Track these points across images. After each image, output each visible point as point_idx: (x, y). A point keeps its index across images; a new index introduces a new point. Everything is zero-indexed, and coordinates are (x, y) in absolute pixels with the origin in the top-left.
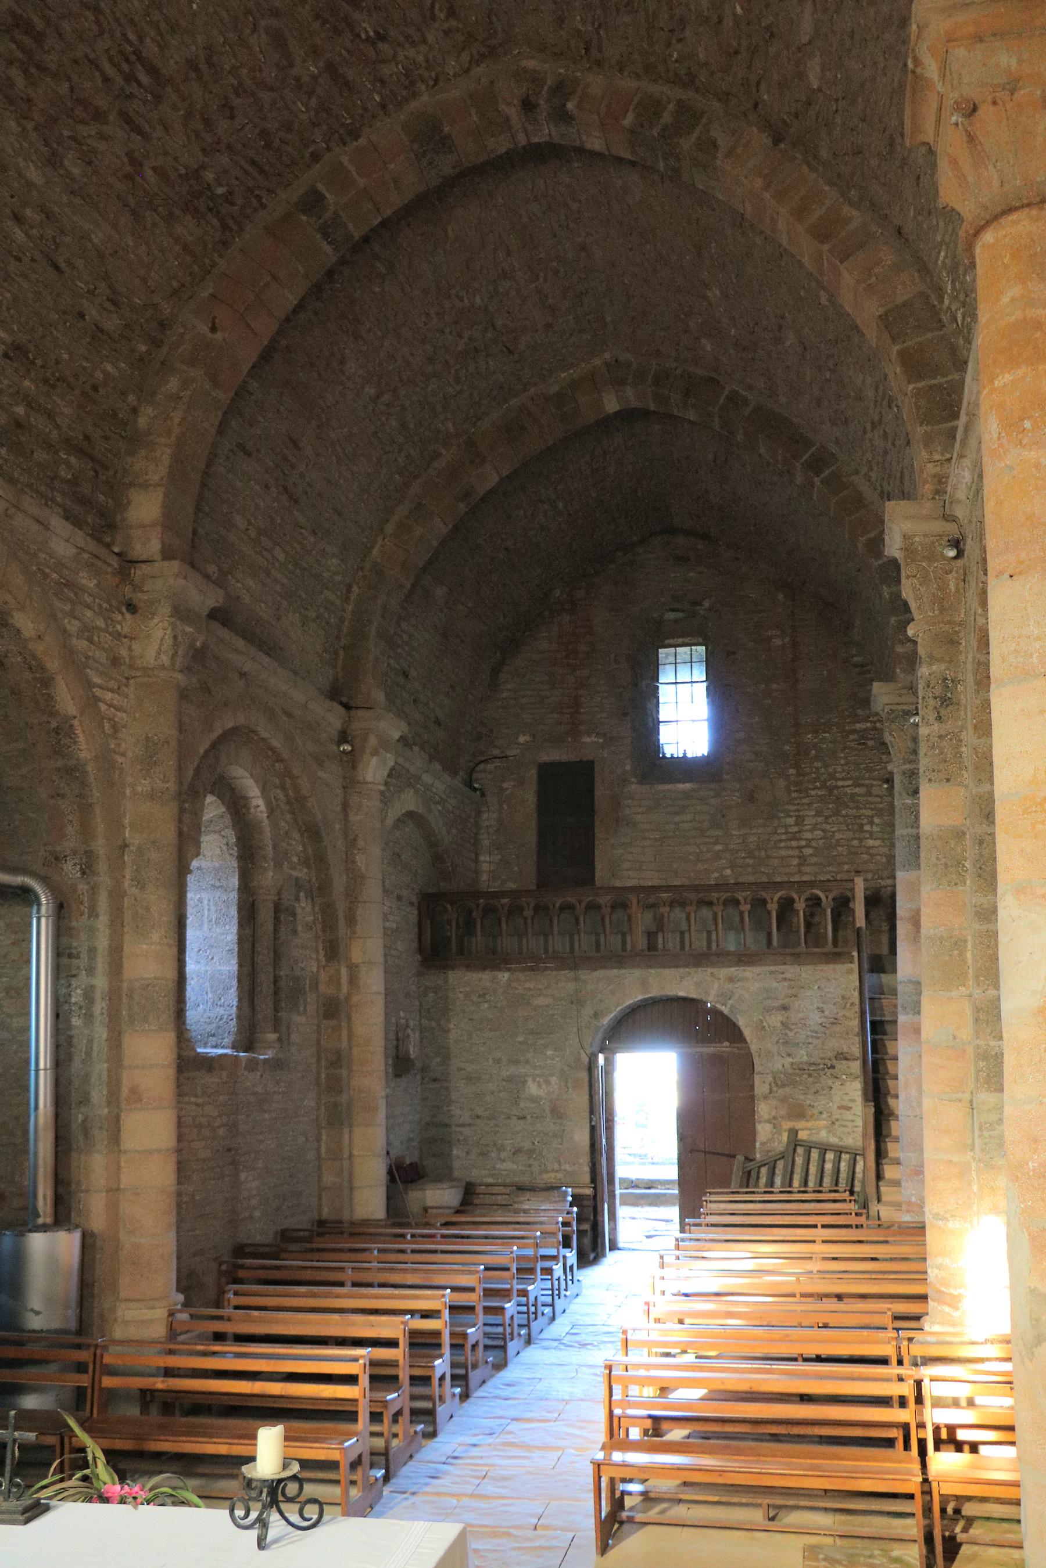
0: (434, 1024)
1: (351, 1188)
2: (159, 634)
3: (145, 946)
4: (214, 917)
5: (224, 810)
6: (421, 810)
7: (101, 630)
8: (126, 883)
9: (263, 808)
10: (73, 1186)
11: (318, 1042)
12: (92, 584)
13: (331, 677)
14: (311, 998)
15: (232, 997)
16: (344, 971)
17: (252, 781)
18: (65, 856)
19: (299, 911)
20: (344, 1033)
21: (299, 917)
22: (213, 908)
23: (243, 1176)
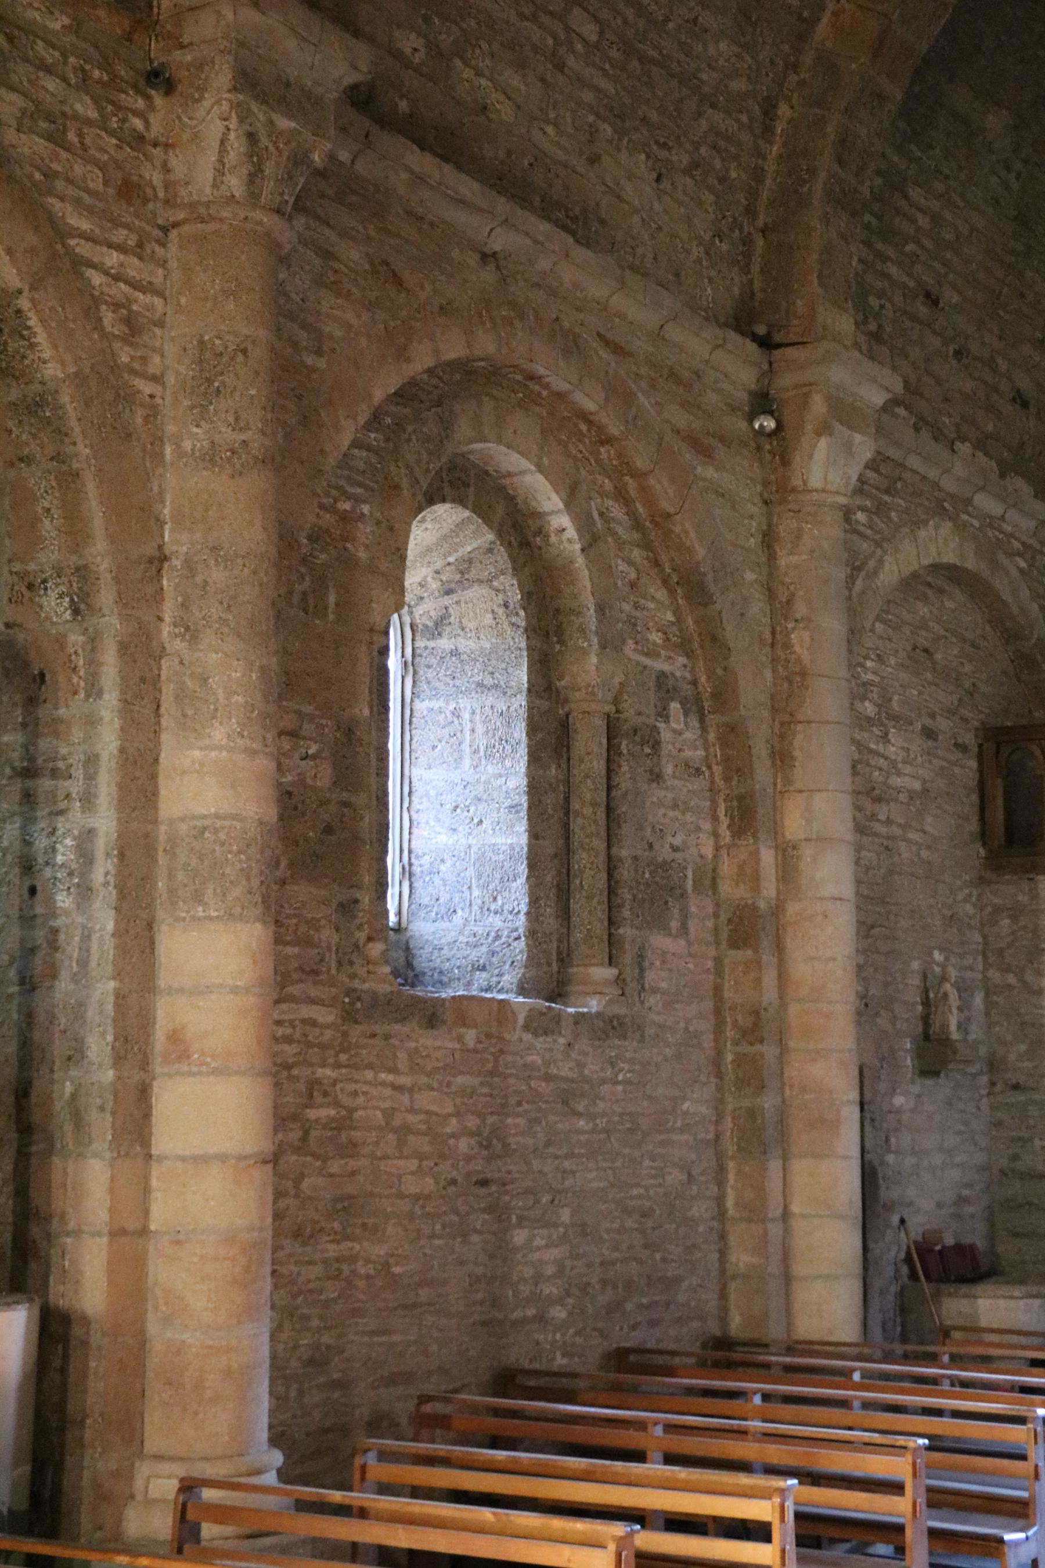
0: (1011, 979)
1: (787, 1278)
2: (216, 129)
3: (197, 753)
4: (482, 742)
5: (491, 537)
6: (971, 563)
7: (89, 122)
8: (166, 630)
9: (571, 532)
10: (55, 1221)
11: (718, 990)
12: (57, 23)
13: (736, 291)
14: (699, 906)
15: (517, 895)
16: (767, 856)
17: (540, 478)
18: (44, 581)
19: (665, 735)
20: (770, 977)
21: (667, 749)
22: (480, 729)
23: (519, 1237)
